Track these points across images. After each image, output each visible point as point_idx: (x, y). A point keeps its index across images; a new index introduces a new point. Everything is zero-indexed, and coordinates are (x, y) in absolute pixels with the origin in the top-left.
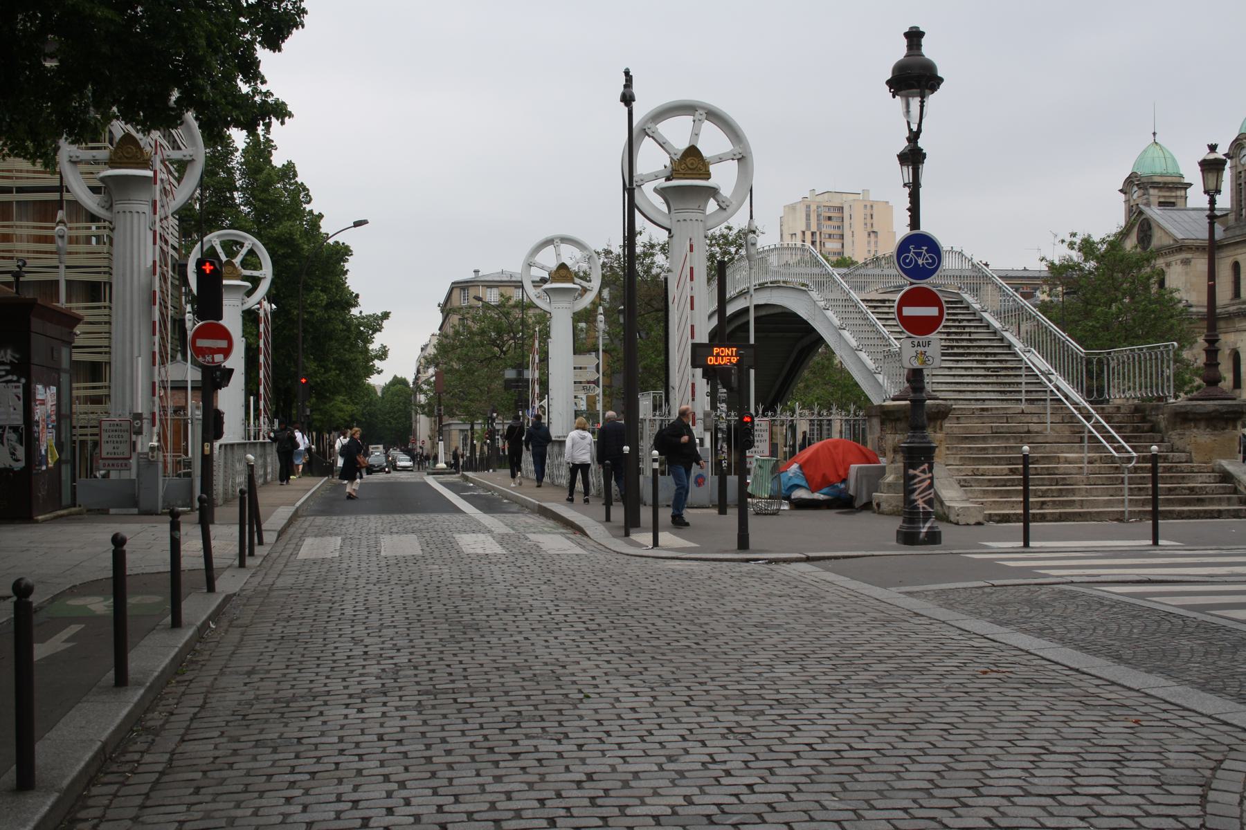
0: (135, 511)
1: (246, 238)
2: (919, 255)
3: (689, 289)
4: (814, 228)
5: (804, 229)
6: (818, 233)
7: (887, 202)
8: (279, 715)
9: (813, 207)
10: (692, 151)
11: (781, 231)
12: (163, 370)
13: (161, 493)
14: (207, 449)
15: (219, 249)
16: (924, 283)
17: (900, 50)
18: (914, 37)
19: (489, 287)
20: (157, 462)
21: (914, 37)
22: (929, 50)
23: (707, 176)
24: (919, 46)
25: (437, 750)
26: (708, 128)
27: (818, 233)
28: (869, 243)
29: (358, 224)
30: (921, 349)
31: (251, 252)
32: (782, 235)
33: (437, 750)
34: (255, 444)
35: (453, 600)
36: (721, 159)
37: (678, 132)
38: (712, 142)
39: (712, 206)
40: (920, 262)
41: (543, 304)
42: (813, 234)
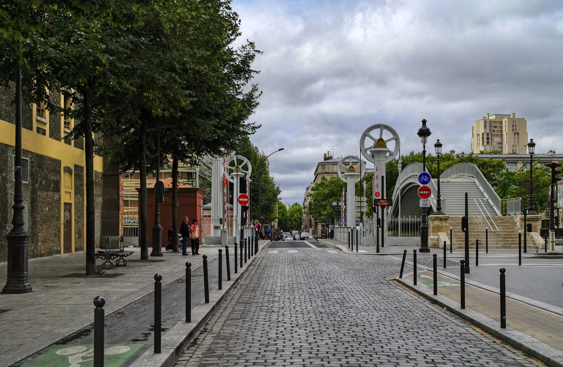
0: (220, 245)
1: (245, 160)
2: (424, 178)
3: (376, 182)
4: (488, 132)
5: (483, 132)
6: (490, 134)
7: (524, 119)
8: (245, 361)
9: (488, 122)
10: (381, 140)
11: (473, 133)
12: (134, 188)
13: (227, 241)
14: (242, 228)
15: (236, 162)
16: (426, 185)
17: (420, 126)
18: (424, 122)
19: (334, 164)
20: (226, 232)
21: (424, 122)
22: (428, 125)
23: (385, 147)
24: (425, 124)
25: (314, 345)
26: (385, 131)
27: (490, 134)
28: (515, 138)
29: (280, 150)
30: (425, 202)
31: (246, 164)
32: (473, 135)
33: (314, 345)
34: (248, 228)
35: (325, 309)
36: (389, 140)
37: (376, 134)
38: (387, 136)
39: (388, 154)
40: (425, 180)
41: (344, 180)
42: (488, 134)
